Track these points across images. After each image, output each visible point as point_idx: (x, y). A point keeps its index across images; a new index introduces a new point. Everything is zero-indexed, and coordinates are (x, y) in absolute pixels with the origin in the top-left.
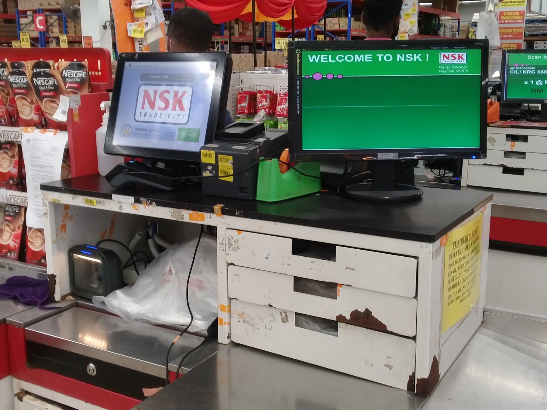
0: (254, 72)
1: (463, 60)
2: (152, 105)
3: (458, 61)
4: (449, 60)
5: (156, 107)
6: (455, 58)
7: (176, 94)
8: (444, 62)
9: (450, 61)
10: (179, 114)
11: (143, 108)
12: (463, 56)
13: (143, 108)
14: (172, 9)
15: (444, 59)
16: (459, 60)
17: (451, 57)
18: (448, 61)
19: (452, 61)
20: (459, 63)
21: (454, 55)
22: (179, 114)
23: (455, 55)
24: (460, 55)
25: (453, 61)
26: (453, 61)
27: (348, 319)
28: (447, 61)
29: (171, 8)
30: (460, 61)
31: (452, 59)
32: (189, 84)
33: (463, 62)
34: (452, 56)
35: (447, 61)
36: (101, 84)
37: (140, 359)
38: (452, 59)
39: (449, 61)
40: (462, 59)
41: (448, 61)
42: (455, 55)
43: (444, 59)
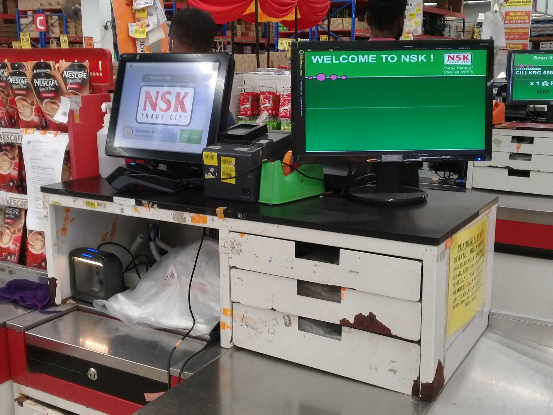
0: (256, 73)
1: (468, 61)
2: (154, 107)
3: (464, 62)
4: (454, 60)
5: (158, 108)
6: (460, 59)
7: (178, 95)
8: (449, 63)
9: (455, 62)
10: (181, 116)
11: (145, 109)
12: (468, 57)
13: (145, 109)
14: (174, 9)
15: (448, 60)
16: (464, 61)
17: (456, 58)
18: (453, 62)
19: (457, 62)
20: (465, 63)
21: (459, 56)
22: (181, 116)
23: (460, 55)
24: (466, 56)
25: (458, 62)
26: (458, 62)
27: (352, 323)
28: (452, 62)
29: (173, 8)
30: (465, 62)
31: (457, 60)
32: (191, 85)
33: (468, 63)
34: (457, 57)
35: (452, 62)
36: (102, 85)
37: (141, 363)
38: (457, 60)
39: (454, 62)
40: (467, 59)
41: (453, 62)
42: (460, 55)
43: (448, 60)
